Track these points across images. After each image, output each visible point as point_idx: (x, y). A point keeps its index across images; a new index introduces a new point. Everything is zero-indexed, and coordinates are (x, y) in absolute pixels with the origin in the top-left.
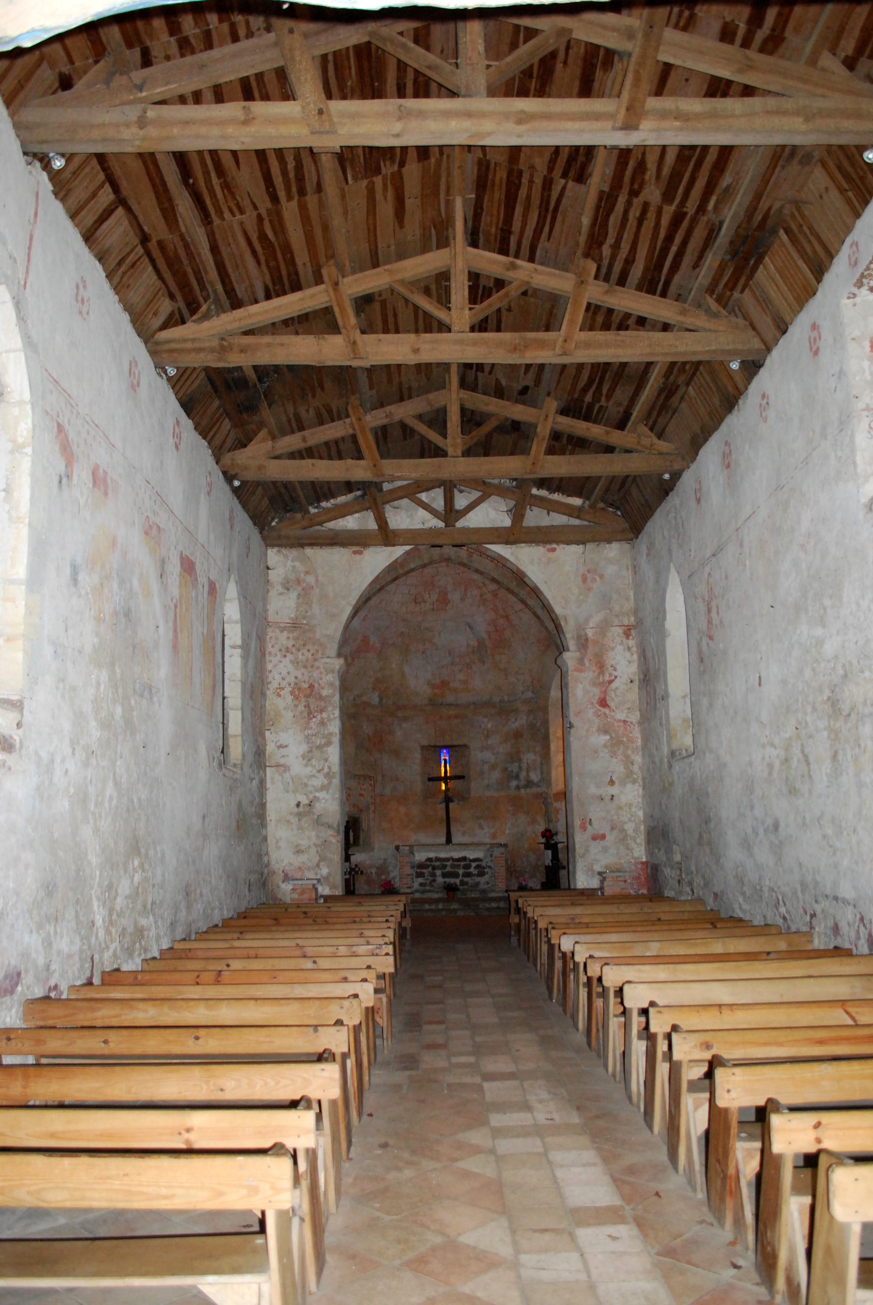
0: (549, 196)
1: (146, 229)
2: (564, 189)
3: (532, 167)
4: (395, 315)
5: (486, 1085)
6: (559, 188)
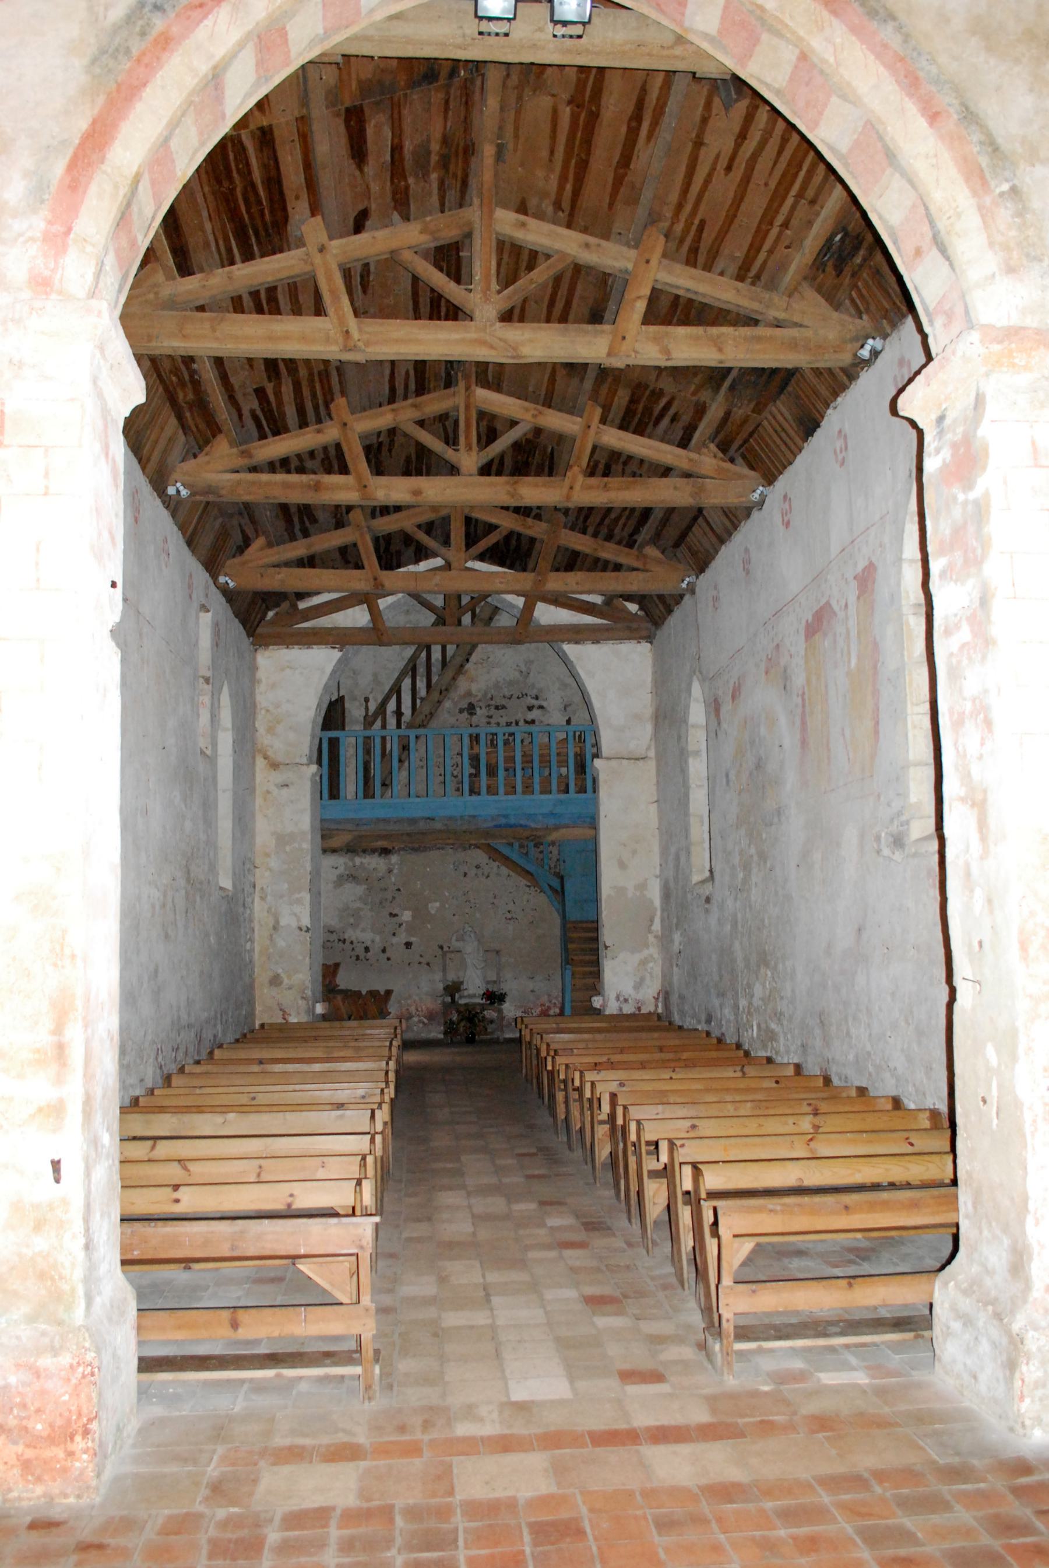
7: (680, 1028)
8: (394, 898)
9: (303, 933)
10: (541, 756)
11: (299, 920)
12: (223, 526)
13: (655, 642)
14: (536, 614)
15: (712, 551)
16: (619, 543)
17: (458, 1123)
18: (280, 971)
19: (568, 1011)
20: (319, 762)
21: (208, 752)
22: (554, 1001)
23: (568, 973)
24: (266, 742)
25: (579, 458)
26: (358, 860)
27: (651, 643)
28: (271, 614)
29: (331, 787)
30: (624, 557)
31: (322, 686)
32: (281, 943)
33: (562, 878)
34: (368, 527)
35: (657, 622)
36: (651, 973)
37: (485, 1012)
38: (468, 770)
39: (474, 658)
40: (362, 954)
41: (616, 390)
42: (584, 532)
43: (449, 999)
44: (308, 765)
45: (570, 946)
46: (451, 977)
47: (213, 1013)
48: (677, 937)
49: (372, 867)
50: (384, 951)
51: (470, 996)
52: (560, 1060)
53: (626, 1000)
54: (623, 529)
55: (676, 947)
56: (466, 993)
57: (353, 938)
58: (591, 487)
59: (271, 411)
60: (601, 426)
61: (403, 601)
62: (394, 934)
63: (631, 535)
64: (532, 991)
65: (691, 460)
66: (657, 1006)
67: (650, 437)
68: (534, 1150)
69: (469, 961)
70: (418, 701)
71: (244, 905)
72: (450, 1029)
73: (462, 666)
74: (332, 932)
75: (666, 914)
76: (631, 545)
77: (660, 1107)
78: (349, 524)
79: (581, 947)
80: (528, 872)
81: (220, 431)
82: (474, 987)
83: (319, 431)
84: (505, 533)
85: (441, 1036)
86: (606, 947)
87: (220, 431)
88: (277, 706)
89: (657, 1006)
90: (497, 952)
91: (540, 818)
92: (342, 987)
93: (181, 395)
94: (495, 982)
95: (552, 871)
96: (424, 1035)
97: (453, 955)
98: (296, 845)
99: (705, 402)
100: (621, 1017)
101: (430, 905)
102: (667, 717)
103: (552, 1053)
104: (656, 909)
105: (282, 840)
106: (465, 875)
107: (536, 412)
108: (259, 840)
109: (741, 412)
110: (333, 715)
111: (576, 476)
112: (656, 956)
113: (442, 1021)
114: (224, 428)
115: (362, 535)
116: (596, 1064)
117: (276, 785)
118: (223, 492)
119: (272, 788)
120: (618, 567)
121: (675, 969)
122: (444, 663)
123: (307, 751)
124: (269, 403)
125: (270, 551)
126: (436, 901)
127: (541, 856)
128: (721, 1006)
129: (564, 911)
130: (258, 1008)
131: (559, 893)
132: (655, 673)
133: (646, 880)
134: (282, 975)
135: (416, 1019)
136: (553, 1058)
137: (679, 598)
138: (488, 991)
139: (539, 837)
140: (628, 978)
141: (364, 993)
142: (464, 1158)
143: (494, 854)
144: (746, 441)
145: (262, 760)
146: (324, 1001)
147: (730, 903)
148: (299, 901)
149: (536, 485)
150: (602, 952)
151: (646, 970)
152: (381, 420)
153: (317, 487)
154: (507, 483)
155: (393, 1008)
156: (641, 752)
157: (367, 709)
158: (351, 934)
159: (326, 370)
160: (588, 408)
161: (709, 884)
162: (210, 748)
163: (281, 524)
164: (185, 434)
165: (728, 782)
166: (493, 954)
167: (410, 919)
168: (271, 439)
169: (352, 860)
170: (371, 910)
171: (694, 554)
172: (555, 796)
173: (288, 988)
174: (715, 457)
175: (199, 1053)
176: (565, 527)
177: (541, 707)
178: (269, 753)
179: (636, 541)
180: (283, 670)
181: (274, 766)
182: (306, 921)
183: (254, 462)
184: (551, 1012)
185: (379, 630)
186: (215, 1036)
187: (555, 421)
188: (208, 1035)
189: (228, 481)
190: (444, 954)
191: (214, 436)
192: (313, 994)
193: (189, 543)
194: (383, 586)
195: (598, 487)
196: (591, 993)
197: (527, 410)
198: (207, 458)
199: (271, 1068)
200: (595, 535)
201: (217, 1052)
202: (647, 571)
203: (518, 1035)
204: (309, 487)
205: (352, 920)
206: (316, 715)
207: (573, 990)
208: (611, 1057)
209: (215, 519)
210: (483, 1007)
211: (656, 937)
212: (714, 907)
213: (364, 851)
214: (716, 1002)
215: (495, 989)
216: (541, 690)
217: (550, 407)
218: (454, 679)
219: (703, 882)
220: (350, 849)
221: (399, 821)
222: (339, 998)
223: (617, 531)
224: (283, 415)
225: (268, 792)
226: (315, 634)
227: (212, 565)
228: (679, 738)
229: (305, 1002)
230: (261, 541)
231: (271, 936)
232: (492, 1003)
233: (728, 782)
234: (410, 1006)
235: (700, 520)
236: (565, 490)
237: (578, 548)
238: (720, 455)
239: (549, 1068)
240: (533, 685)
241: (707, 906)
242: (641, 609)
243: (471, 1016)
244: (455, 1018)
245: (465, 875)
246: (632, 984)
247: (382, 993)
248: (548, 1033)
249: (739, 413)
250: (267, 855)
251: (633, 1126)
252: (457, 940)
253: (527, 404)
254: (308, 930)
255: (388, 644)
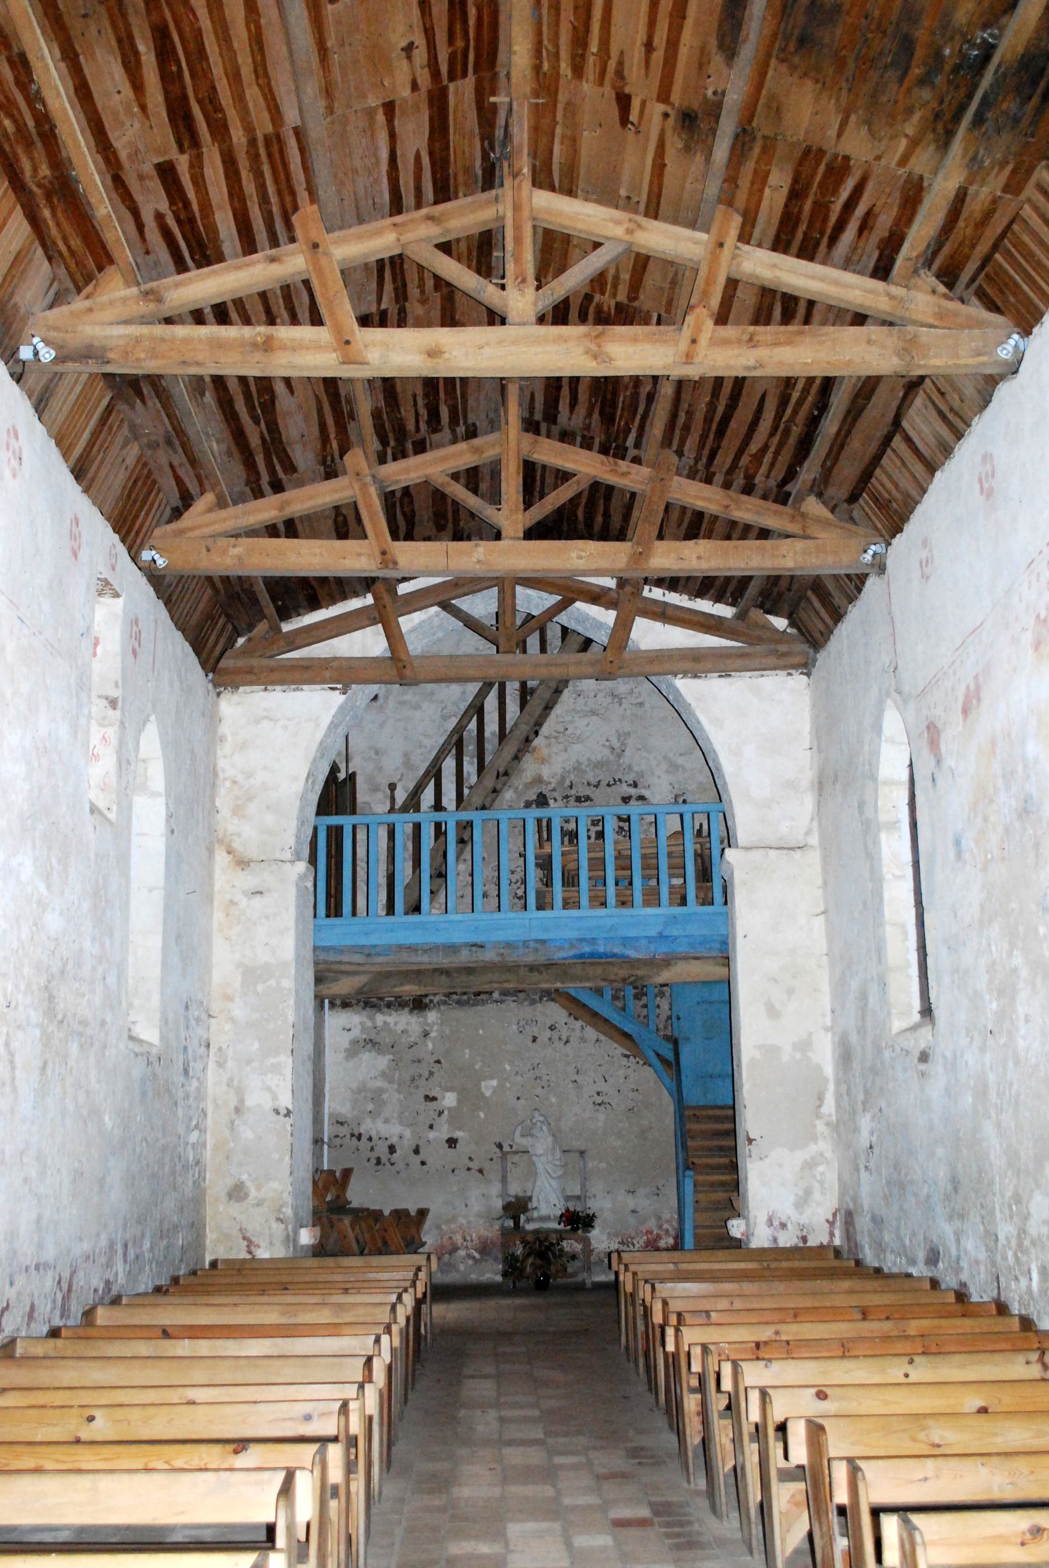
0: (394, 280)
1: (901, 394)
2: (379, 300)
3: (423, 301)
4: (649, 46)
5: (542, 1436)
6: (385, 298)
7: (878, 1271)
8: (431, 1073)
9: (281, 1117)
10: (644, 857)
11: (275, 1098)
12: (142, 462)
13: (814, 671)
14: (633, 635)
15: (914, 493)
16: (764, 497)
17: (510, 1443)
18: (244, 1177)
19: (689, 1242)
20: (313, 860)
21: (112, 816)
22: (665, 1226)
23: (689, 1187)
24: (231, 828)
25: (705, 294)
26: (380, 1019)
27: (808, 675)
28: (241, 641)
29: (333, 898)
30: (770, 517)
31: (315, 746)
32: (247, 1134)
33: (675, 1042)
34: (373, 476)
35: (815, 639)
36: (822, 1183)
37: (564, 1243)
38: (534, 875)
39: (545, 730)
40: (385, 1156)
41: (767, 174)
42: (708, 480)
43: (511, 1223)
44: (292, 862)
45: (690, 1143)
46: (515, 1189)
47: (103, 1242)
48: (865, 1123)
49: (400, 1028)
50: (417, 1151)
51: (542, 1219)
52: (691, 1336)
53: (783, 1226)
54: (768, 477)
55: (864, 1138)
56: (535, 1214)
57: (373, 1134)
58: (726, 342)
59: (192, 220)
60: (739, 244)
61: (436, 621)
62: (431, 1127)
63: (785, 482)
64: (633, 1212)
65: (892, 298)
66: (832, 1235)
67: (824, 263)
68: (644, 1512)
69: (540, 1167)
70: (466, 791)
71: (186, 1072)
72: (512, 1267)
73: (528, 740)
74: (342, 1124)
75: (844, 1088)
76: (783, 499)
77: (930, 1463)
78: (345, 473)
79: (709, 1144)
80: (627, 1036)
81: (111, 261)
82: (548, 1205)
83: (273, 260)
84: (585, 485)
85: (499, 1278)
86: (750, 1141)
87: (111, 261)
88: (249, 775)
89: (832, 1235)
90: (582, 1153)
91: (644, 942)
92: (355, 1205)
93: (26, 165)
94: (578, 1198)
95: (662, 1033)
96: (474, 1277)
97: (516, 1158)
98: (273, 983)
99: (921, 178)
100: (776, 1253)
101: (483, 1084)
102: (839, 775)
103: (673, 1319)
104: (827, 1080)
105: (251, 974)
106: (535, 1039)
107: (632, 226)
108: (217, 976)
109: (985, 190)
110: (336, 793)
111: (701, 320)
112: (829, 1154)
113: (500, 1256)
114: (115, 254)
115: (364, 487)
116: (758, 1345)
117: (244, 893)
118: (111, 355)
119: (239, 897)
120: (764, 534)
121: (864, 1175)
122: (502, 735)
123: (292, 841)
124: (187, 204)
125: (223, 514)
126: (493, 1078)
127: (644, 1012)
128: (958, 1236)
129: (680, 1092)
130: (210, 1236)
131: (672, 1065)
132: (815, 719)
133: (810, 1034)
134: (248, 1184)
135: (462, 1253)
136: (677, 1330)
137: (858, 581)
138: (567, 1210)
139: (642, 978)
140: (784, 1192)
141: (386, 1213)
142: (514, 1529)
143: (577, 1008)
144: (987, 259)
145: (225, 854)
146: (314, 1226)
147: (970, 1058)
148: (276, 1069)
149: (635, 340)
150: (742, 1147)
151: (814, 1177)
152: (378, 241)
153: (268, 346)
154: (587, 335)
155: (429, 1237)
156: (798, 838)
157: (393, 799)
158: (368, 1126)
159: (278, 136)
160: (719, 216)
161: (926, 1032)
162: (114, 808)
163: (238, 469)
164: (50, 259)
165: (959, 855)
166: (575, 1156)
167: (454, 1104)
168: (194, 273)
169: (372, 1018)
170: (399, 1092)
171: (882, 505)
172: (666, 910)
173: (261, 1206)
174: (934, 292)
175: (64, 1313)
176: (679, 474)
177: (641, 798)
178: (235, 845)
179: (789, 494)
180: (257, 721)
181: (243, 863)
182: (286, 1100)
183: (166, 310)
184: (662, 1244)
185: (400, 660)
186: (108, 1283)
187: (662, 238)
188: (90, 1281)
189: (120, 337)
190: (504, 1156)
191: (101, 269)
192: (296, 1214)
193: (79, 473)
194: (395, 563)
195: (739, 341)
196: (726, 1214)
197: (618, 222)
198: (87, 303)
199: (183, 1347)
200: (727, 485)
201: (100, 1311)
202: (806, 537)
203: (613, 1277)
204: (255, 345)
205: (370, 1107)
206: (306, 790)
207: (696, 1210)
208: (783, 1328)
209: (126, 444)
210: (561, 1236)
211: (827, 1124)
212: (936, 1067)
213: (389, 1006)
214: (947, 1229)
215: (578, 1209)
216: (641, 774)
217: (656, 218)
218: (517, 758)
219: (914, 1028)
220: (367, 1000)
221: (435, 948)
222: (347, 1221)
223: (759, 479)
224: (212, 229)
225: (232, 903)
226: (307, 668)
227: (128, 525)
228: (861, 805)
229: (282, 1226)
230: (209, 497)
231: (232, 1122)
232: (575, 1230)
233: (959, 855)
234: (454, 1232)
235: (897, 441)
236: (683, 345)
237: (700, 505)
238: (942, 289)
239: (670, 1347)
240: (630, 767)
241: (922, 1067)
242: (792, 624)
243: (543, 1248)
244: (519, 1251)
245: (535, 1039)
246: (792, 1199)
247: (413, 1213)
248: (663, 1281)
249: (982, 195)
250: (230, 999)
251: (840, 1473)
252: (523, 1136)
253: (616, 214)
254: (288, 1113)
255: (416, 683)
